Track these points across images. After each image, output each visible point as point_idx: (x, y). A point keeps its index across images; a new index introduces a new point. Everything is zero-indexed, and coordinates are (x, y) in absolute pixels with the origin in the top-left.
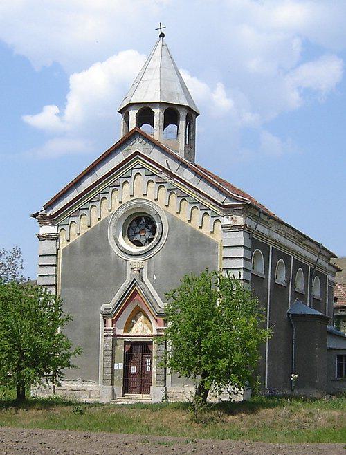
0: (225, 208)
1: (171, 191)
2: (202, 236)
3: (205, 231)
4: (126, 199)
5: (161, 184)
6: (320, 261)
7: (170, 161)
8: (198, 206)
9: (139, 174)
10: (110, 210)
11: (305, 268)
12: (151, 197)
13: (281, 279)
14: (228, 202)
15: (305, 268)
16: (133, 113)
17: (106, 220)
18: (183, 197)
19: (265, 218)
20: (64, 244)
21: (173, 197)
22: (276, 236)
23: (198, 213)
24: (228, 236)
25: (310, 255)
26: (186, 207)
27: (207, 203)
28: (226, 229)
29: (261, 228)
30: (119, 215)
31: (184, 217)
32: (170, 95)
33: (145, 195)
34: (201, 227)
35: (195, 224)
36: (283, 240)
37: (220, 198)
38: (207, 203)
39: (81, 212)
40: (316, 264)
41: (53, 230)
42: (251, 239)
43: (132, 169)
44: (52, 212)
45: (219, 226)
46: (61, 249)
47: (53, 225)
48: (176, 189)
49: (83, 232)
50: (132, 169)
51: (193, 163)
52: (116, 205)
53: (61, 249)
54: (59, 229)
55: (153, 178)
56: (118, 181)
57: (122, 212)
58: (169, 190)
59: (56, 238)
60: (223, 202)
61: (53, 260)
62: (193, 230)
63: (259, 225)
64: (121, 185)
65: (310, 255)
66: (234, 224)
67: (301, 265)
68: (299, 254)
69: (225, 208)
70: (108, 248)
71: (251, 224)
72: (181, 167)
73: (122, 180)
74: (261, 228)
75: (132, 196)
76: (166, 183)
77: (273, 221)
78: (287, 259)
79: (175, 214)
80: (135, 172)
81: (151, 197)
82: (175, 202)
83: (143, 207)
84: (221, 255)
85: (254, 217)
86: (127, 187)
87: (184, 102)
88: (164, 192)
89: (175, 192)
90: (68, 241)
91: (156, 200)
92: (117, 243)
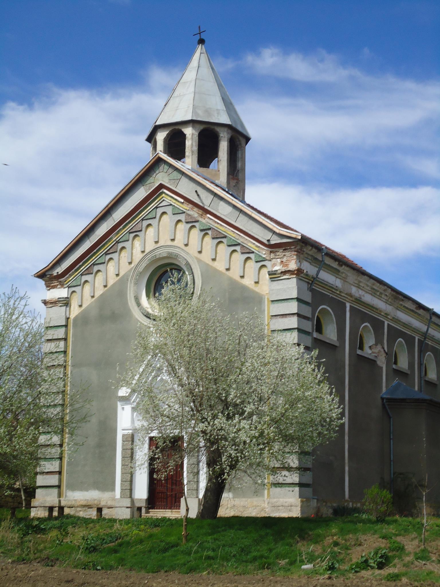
0: (273, 247)
1: (205, 231)
2: (244, 288)
3: (248, 282)
4: (150, 246)
5: (192, 223)
6: (431, 332)
7: (201, 191)
8: (238, 248)
9: (164, 213)
10: (130, 263)
11: (409, 340)
12: (180, 241)
13: (403, 363)
14: (275, 240)
15: (409, 340)
16: (161, 137)
17: (126, 275)
18: (219, 238)
19: (335, 265)
20: (75, 311)
21: (208, 239)
22: (354, 290)
23: (238, 258)
24: (278, 285)
25: (416, 323)
26: (223, 250)
27: (251, 245)
28: (274, 276)
29: (325, 276)
30: (141, 269)
31: (220, 265)
32: (207, 111)
33: (173, 240)
34: (242, 277)
35: (235, 274)
36: (368, 298)
37: (264, 236)
38: (251, 245)
39: (96, 268)
40: (425, 335)
41: (62, 293)
42: (311, 290)
43: (157, 207)
44: (60, 270)
45: (265, 274)
46: (72, 316)
47: (62, 285)
48: (209, 229)
49: (98, 294)
50: (157, 207)
51: (243, 201)
52: (138, 256)
53: (72, 316)
54: (70, 293)
55: (182, 217)
56: (140, 225)
57: (144, 265)
58: (202, 230)
59: (66, 302)
60: (268, 241)
61: (60, 333)
62: (233, 283)
63: (321, 271)
64: (144, 229)
65: (416, 323)
66: (284, 269)
67: (365, 317)
68: (396, 320)
69: (273, 247)
70: (128, 313)
71: (309, 269)
72: (216, 199)
73: (145, 223)
74: (325, 276)
75: (157, 242)
76: (197, 221)
77: (347, 269)
78: (377, 325)
79: (210, 263)
80: (160, 211)
81: (180, 241)
82: (209, 247)
83: (170, 256)
84: (268, 313)
85: (314, 261)
86: (151, 231)
87: (224, 119)
88: (196, 234)
89: (210, 232)
90: (80, 306)
91: (186, 245)
92: (139, 304)
